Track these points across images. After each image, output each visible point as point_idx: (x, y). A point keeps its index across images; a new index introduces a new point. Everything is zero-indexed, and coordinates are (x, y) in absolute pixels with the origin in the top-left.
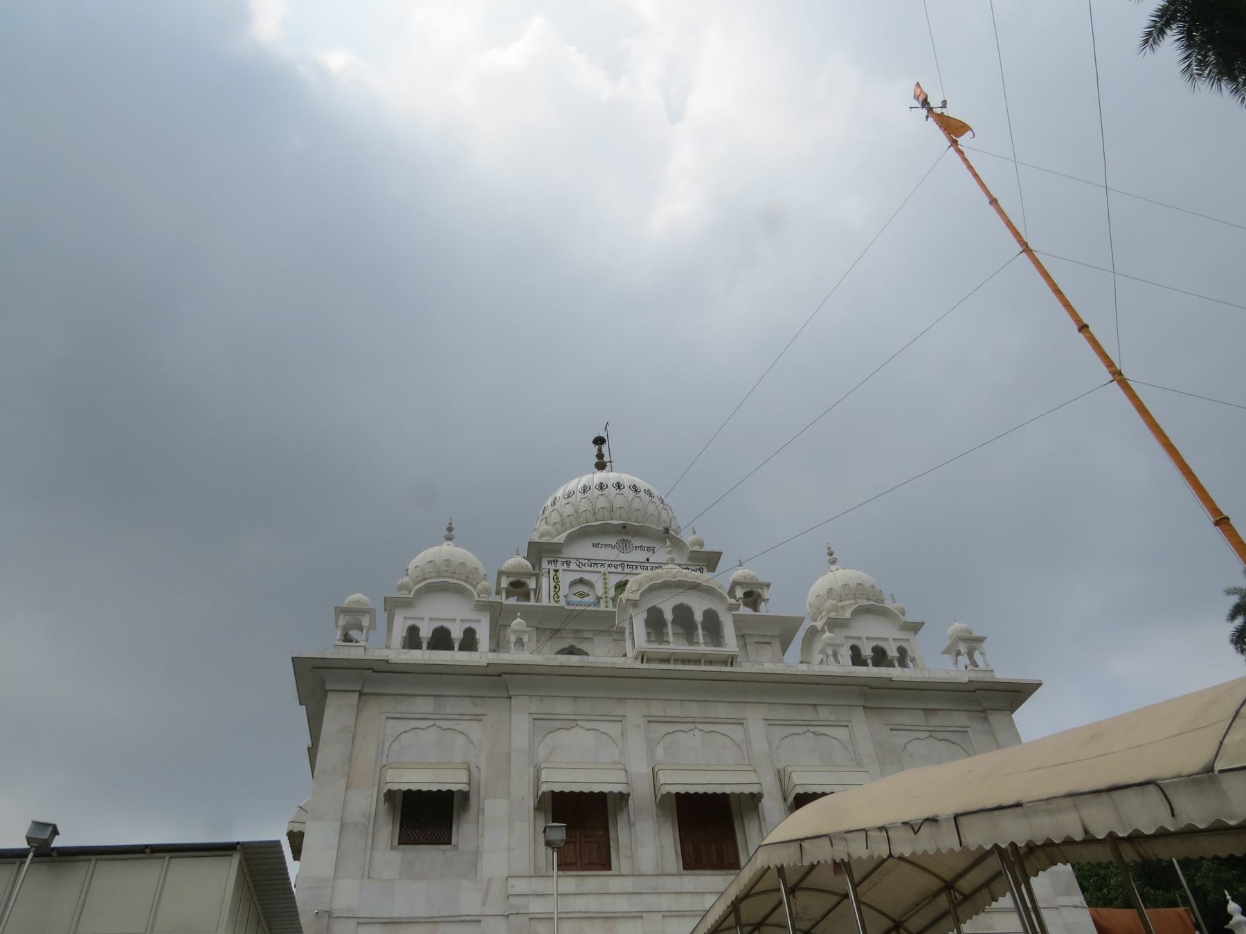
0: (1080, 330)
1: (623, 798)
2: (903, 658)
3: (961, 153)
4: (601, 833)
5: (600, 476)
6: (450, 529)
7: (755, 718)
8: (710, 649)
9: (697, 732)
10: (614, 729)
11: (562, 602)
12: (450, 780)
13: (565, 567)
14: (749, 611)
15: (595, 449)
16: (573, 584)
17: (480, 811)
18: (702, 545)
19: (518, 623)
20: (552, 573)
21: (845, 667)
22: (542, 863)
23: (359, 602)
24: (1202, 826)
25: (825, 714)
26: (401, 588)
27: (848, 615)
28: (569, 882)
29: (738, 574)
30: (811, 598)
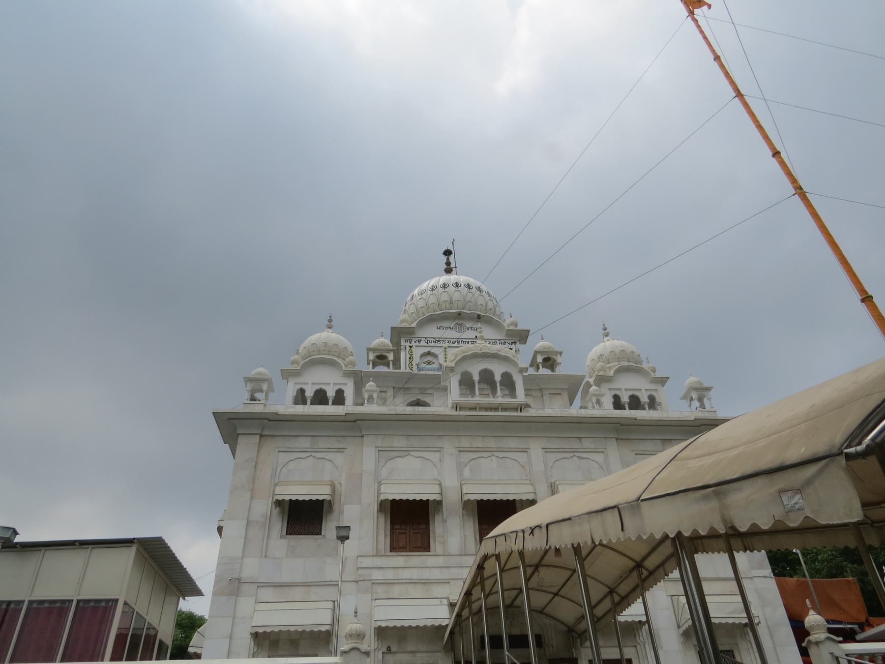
0: (774, 156)
1: (439, 503)
2: (653, 403)
3: (696, 21)
4: (423, 526)
5: (452, 278)
6: (330, 321)
7: (536, 448)
8: (508, 400)
9: (494, 458)
10: (434, 457)
11: (415, 367)
12: (319, 493)
13: (417, 344)
14: (547, 372)
15: (445, 258)
16: (423, 355)
17: (341, 512)
18: (516, 325)
19: (370, 385)
20: (408, 348)
21: (608, 410)
22: (381, 547)
23: (260, 373)
24: (703, 533)
25: (587, 444)
26: (293, 363)
27: (611, 373)
28: (399, 560)
29: (540, 345)
30: (588, 362)
